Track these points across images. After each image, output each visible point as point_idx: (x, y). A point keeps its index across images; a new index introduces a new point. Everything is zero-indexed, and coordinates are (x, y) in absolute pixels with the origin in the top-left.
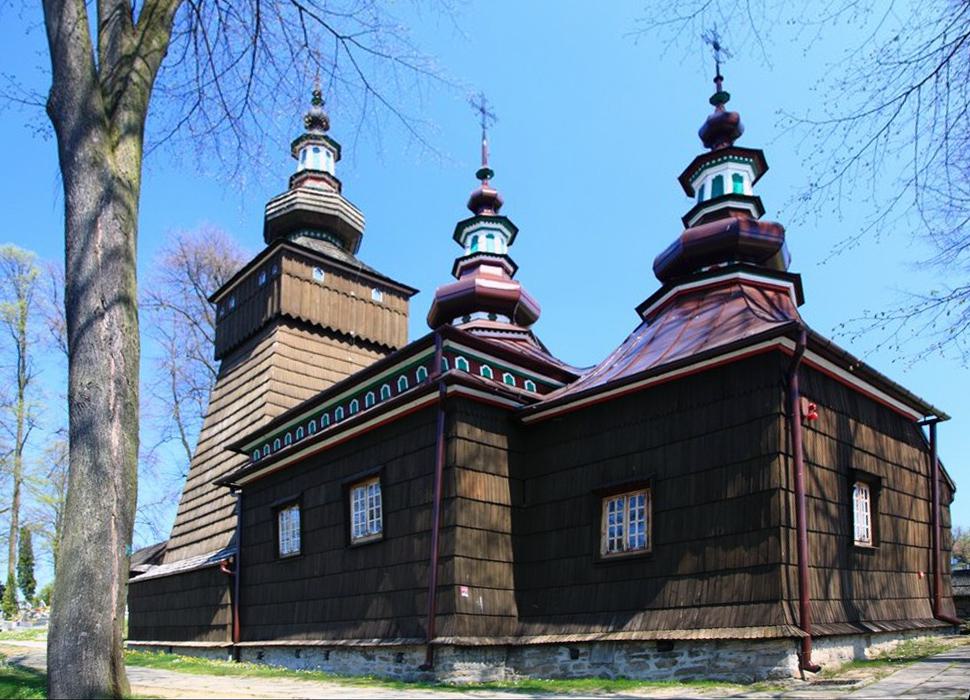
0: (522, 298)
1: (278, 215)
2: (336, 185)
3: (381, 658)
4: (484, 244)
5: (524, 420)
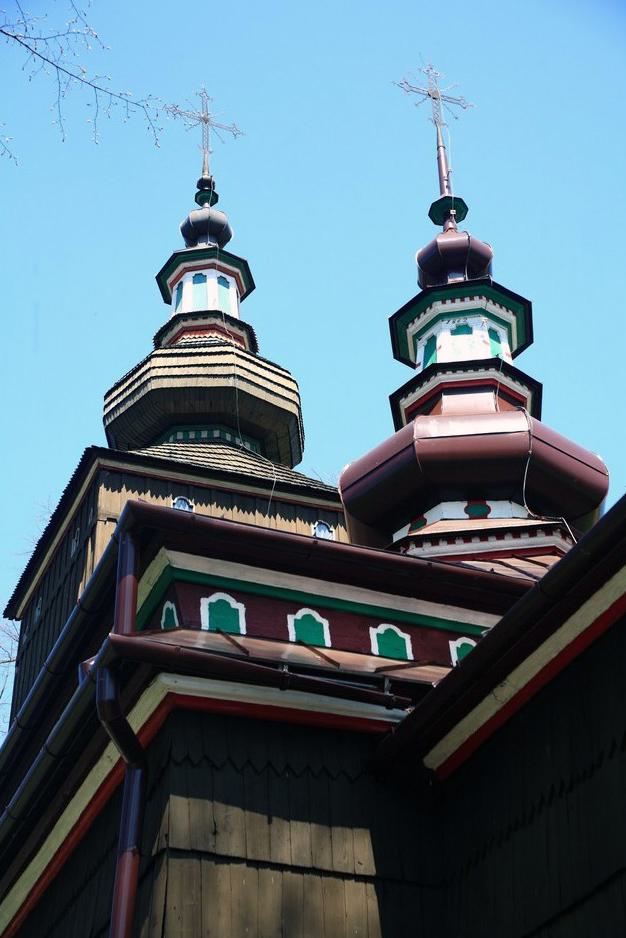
1: (122, 410)
2: (243, 334)
4: (451, 347)
5: (437, 756)
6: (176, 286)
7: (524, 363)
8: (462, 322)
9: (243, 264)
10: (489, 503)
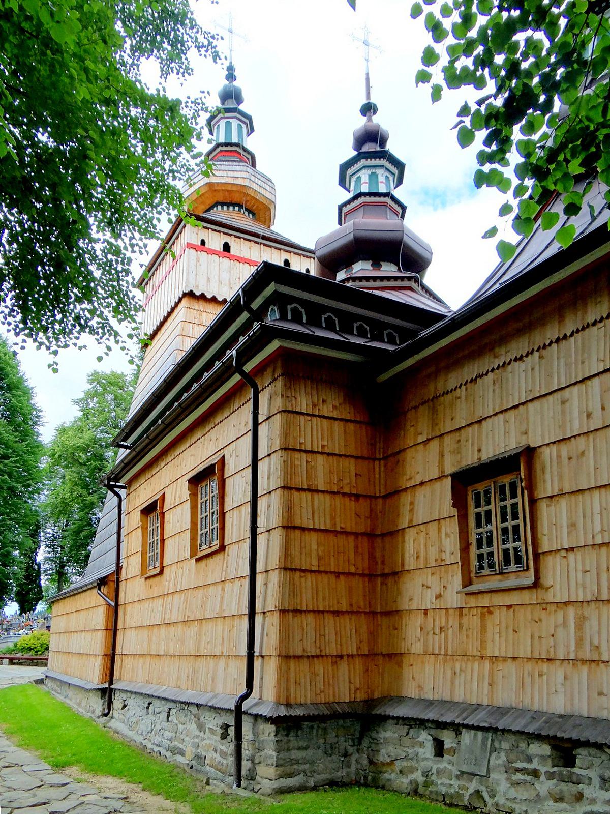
0: (406, 238)
3: (182, 753)
6: (216, 126)
7: (398, 193)
8: (374, 171)
9: (249, 118)
10: (381, 263)
